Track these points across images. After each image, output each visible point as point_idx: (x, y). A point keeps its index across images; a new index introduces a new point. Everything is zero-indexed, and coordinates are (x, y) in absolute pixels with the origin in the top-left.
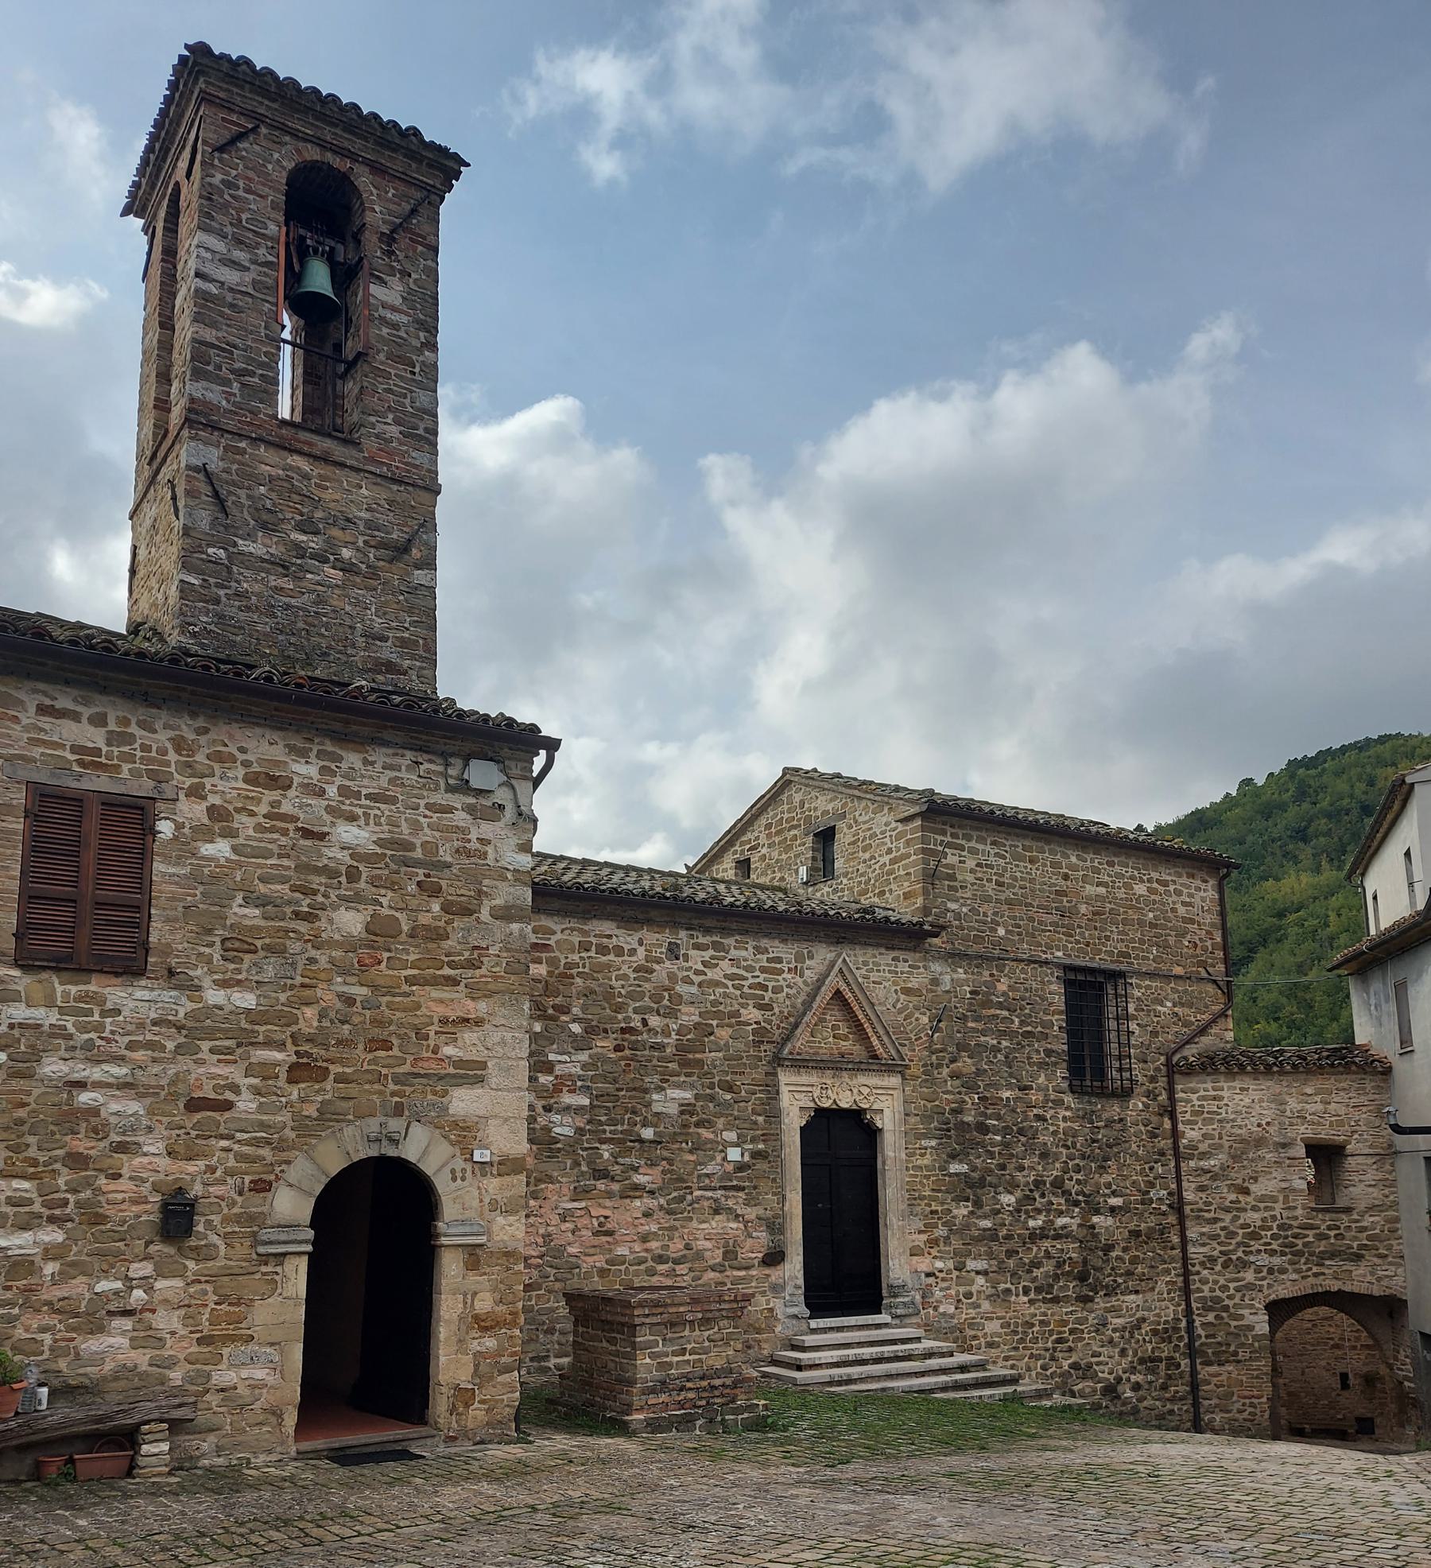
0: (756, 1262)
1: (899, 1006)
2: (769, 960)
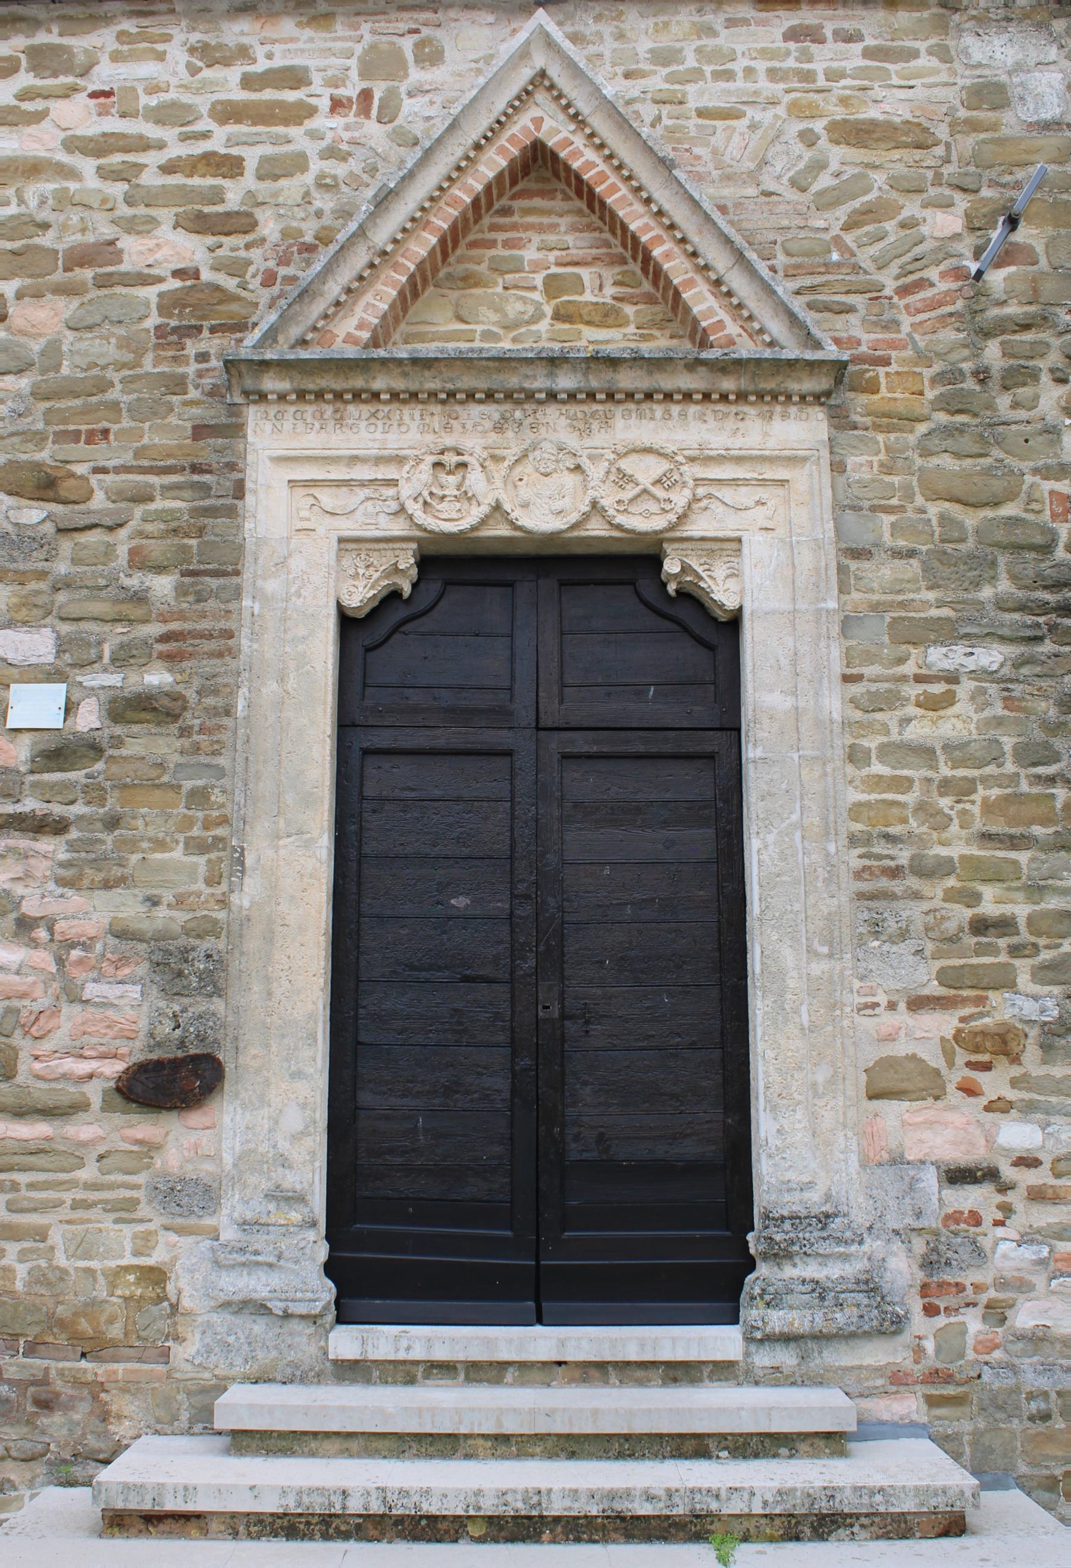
0: (94, 1093)
1: (825, 181)
2: (248, 82)
